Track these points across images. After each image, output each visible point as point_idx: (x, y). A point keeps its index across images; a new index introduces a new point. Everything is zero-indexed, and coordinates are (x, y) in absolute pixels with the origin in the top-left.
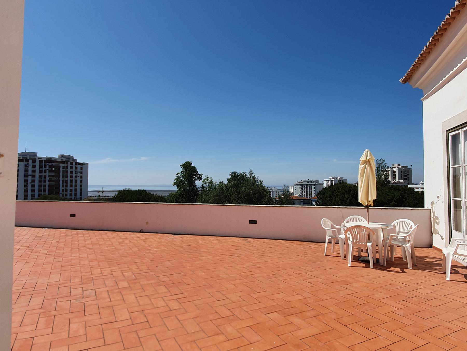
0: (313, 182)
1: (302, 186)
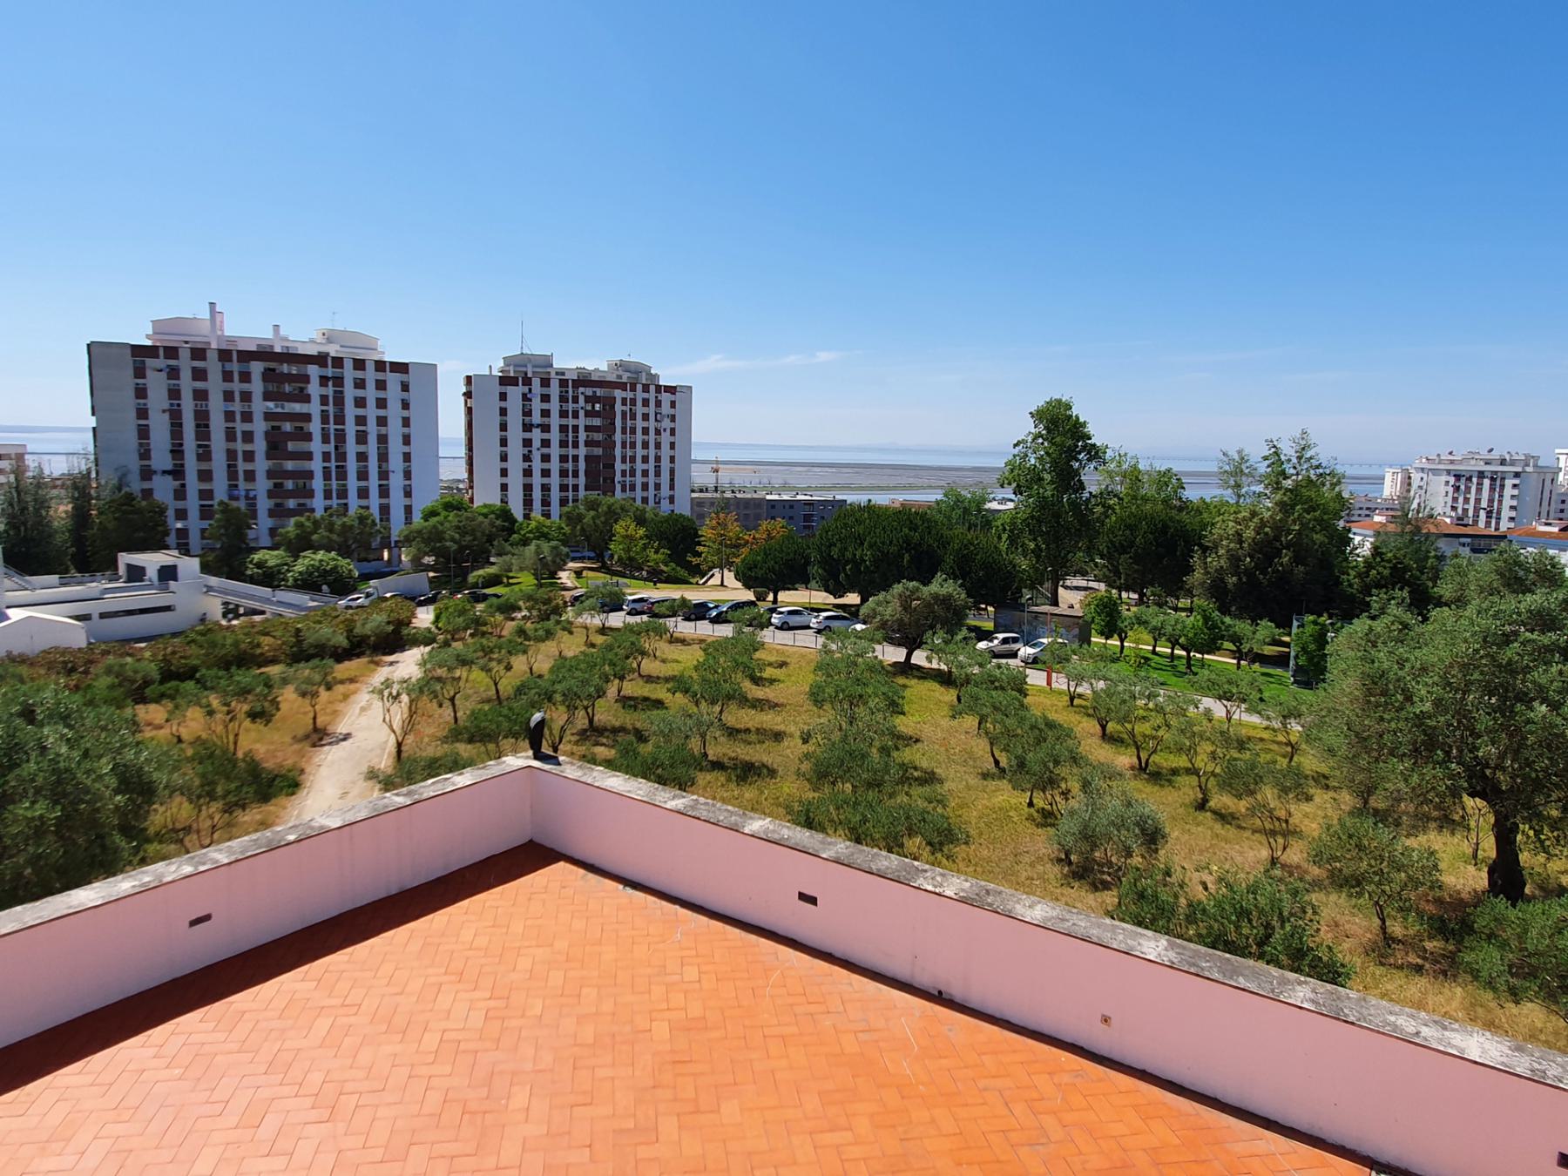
0: (1513, 463)
1: (1458, 477)
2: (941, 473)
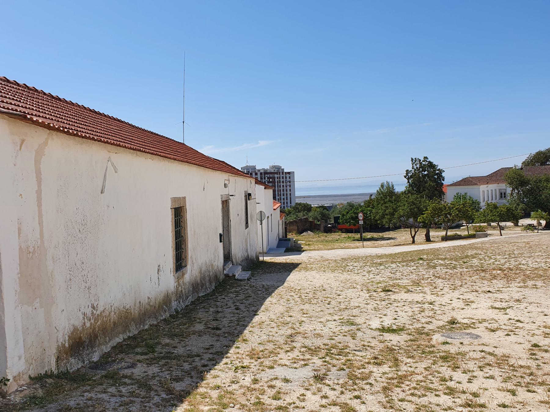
2: (344, 198)
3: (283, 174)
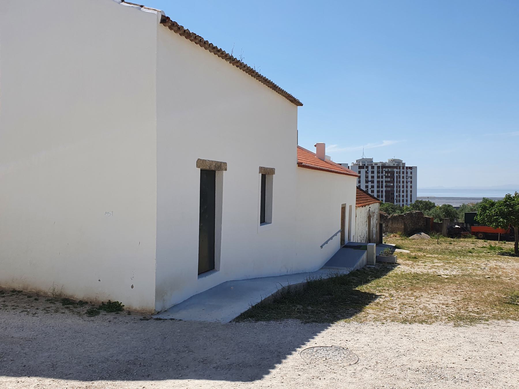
3: (403, 168)
